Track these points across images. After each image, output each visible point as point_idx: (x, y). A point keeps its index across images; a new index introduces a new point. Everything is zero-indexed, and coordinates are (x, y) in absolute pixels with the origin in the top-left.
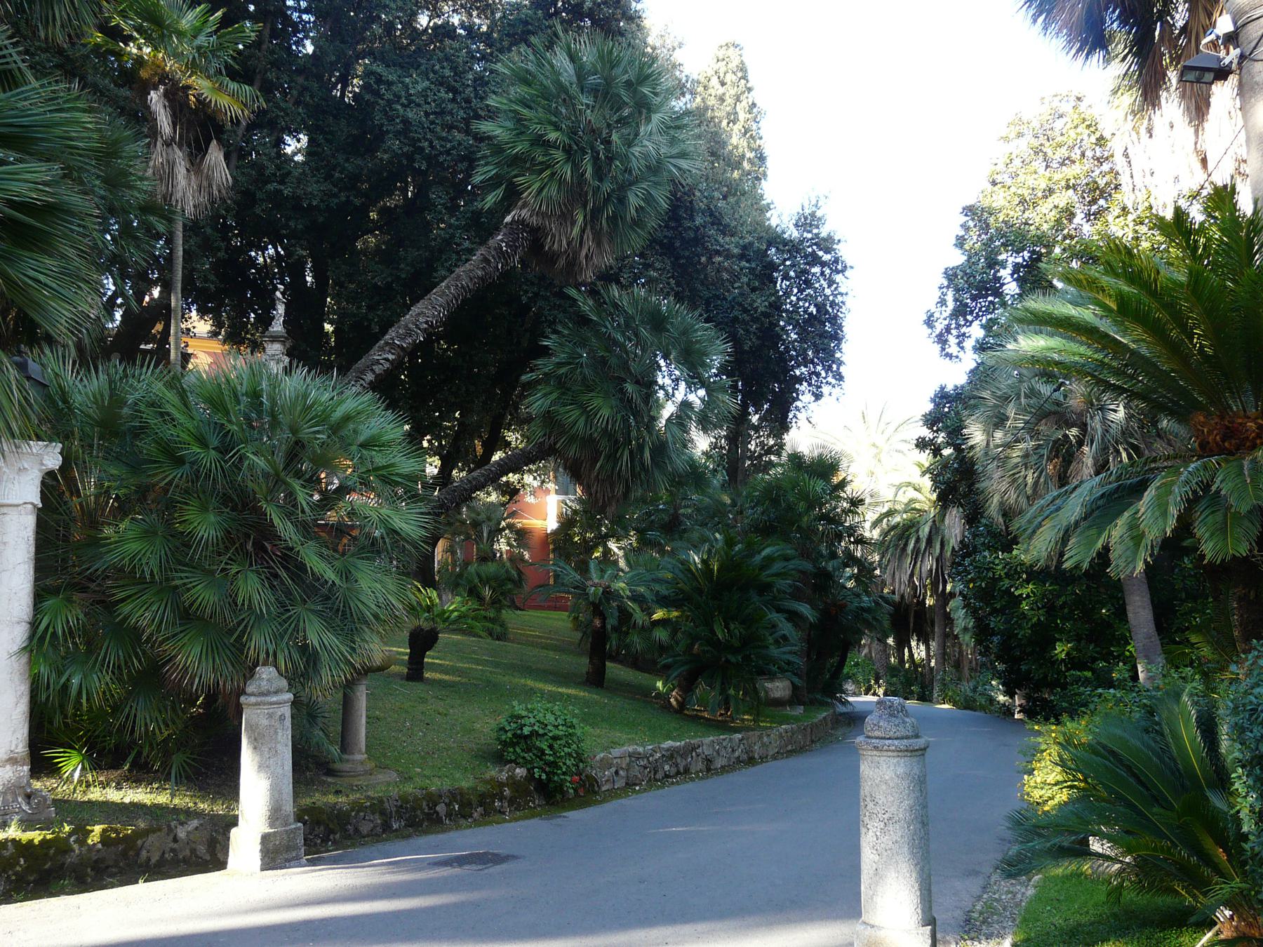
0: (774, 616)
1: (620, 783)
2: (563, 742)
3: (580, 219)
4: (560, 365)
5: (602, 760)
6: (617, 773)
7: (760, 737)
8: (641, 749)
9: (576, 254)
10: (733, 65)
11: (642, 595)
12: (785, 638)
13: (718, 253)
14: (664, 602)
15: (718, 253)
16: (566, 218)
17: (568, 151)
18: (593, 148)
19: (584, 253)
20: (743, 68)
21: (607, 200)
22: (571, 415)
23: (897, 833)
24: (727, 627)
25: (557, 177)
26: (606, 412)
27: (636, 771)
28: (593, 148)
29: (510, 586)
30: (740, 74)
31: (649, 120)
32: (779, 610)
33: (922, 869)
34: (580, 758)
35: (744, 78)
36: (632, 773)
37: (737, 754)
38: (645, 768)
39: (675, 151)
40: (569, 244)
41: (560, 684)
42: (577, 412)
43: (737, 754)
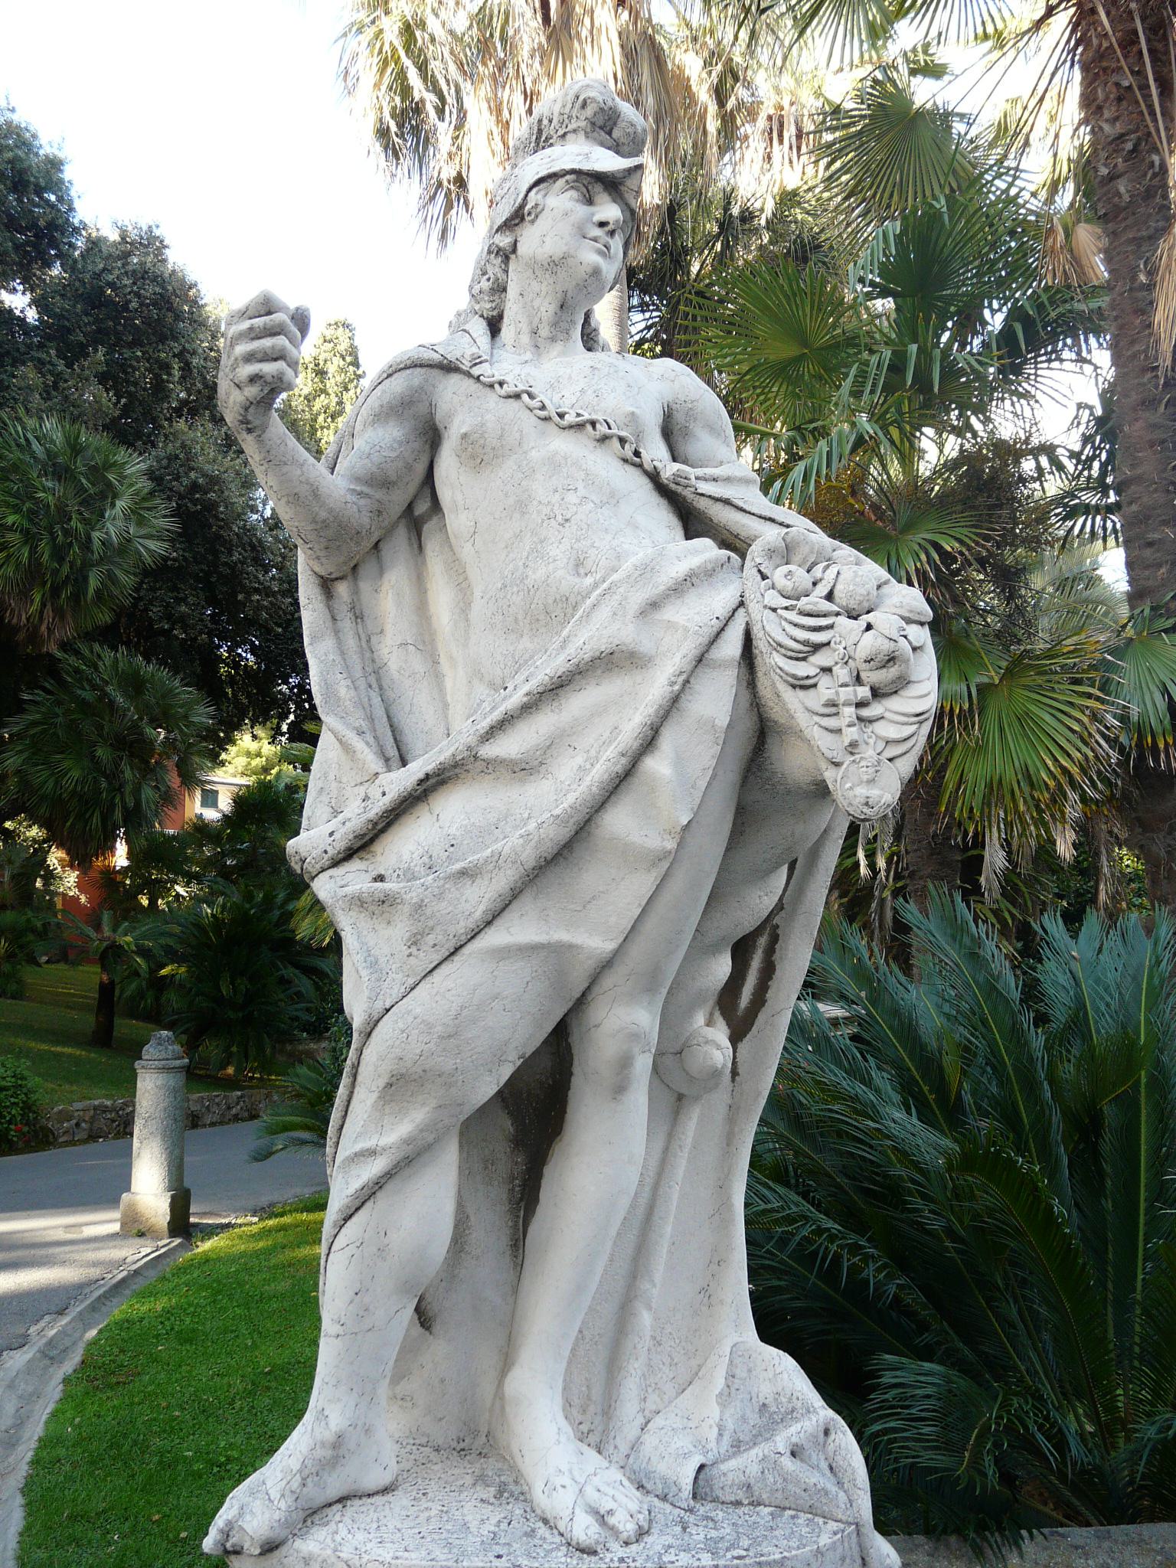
0: (289, 972)
1: (83, 1135)
2: (10, 1093)
3: (38, 598)
4: (34, 724)
5: (60, 1112)
6: (77, 1125)
7: (268, 1096)
8: (109, 1103)
9: (36, 628)
10: (343, 347)
11: (150, 950)
12: (299, 994)
13: (257, 591)
14: (173, 956)
15: (257, 591)
16: (25, 595)
17: (27, 534)
18: (51, 533)
19: (43, 628)
20: (353, 351)
21: (66, 582)
22: (40, 776)
23: (154, 1125)
24: (232, 983)
25: (13, 560)
26: (76, 774)
27: (101, 1123)
28: (51, 533)
29: (31, 937)
30: (349, 359)
31: (113, 505)
32: (297, 966)
33: (171, 1153)
34: (27, 1107)
35: (356, 364)
36: (96, 1125)
37: (234, 1111)
38: (114, 1121)
39: (143, 532)
40: (28, 619)
41: (57, 1043)
42: (46, 773)
43: (234, 1111)
